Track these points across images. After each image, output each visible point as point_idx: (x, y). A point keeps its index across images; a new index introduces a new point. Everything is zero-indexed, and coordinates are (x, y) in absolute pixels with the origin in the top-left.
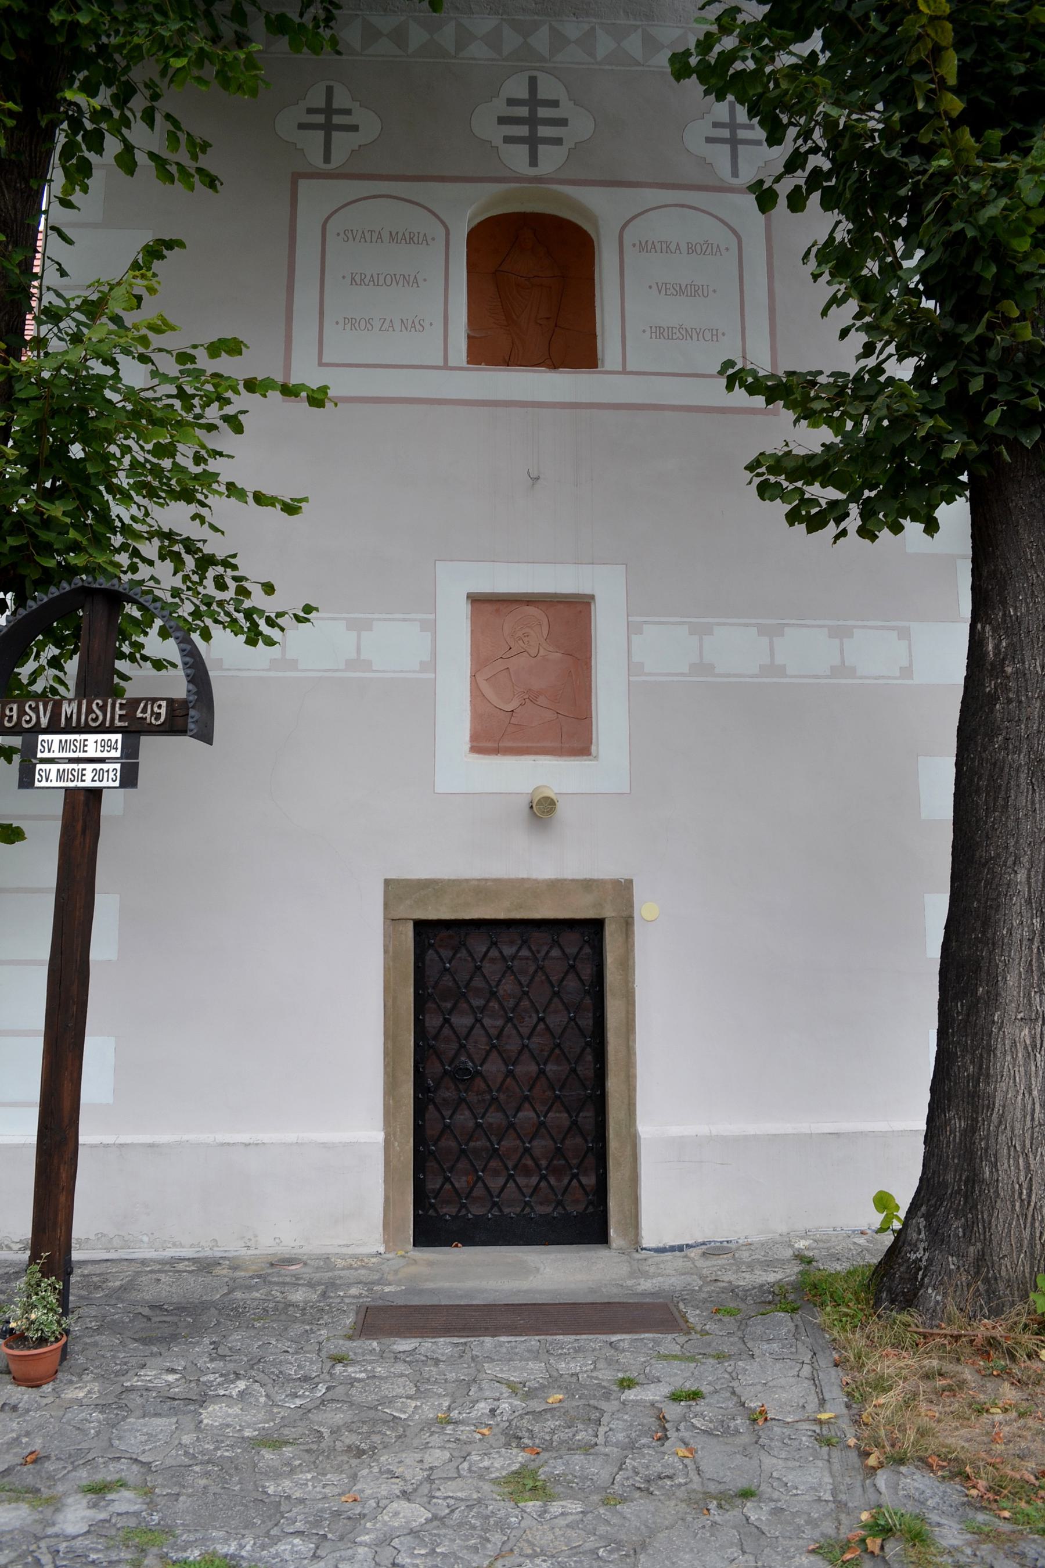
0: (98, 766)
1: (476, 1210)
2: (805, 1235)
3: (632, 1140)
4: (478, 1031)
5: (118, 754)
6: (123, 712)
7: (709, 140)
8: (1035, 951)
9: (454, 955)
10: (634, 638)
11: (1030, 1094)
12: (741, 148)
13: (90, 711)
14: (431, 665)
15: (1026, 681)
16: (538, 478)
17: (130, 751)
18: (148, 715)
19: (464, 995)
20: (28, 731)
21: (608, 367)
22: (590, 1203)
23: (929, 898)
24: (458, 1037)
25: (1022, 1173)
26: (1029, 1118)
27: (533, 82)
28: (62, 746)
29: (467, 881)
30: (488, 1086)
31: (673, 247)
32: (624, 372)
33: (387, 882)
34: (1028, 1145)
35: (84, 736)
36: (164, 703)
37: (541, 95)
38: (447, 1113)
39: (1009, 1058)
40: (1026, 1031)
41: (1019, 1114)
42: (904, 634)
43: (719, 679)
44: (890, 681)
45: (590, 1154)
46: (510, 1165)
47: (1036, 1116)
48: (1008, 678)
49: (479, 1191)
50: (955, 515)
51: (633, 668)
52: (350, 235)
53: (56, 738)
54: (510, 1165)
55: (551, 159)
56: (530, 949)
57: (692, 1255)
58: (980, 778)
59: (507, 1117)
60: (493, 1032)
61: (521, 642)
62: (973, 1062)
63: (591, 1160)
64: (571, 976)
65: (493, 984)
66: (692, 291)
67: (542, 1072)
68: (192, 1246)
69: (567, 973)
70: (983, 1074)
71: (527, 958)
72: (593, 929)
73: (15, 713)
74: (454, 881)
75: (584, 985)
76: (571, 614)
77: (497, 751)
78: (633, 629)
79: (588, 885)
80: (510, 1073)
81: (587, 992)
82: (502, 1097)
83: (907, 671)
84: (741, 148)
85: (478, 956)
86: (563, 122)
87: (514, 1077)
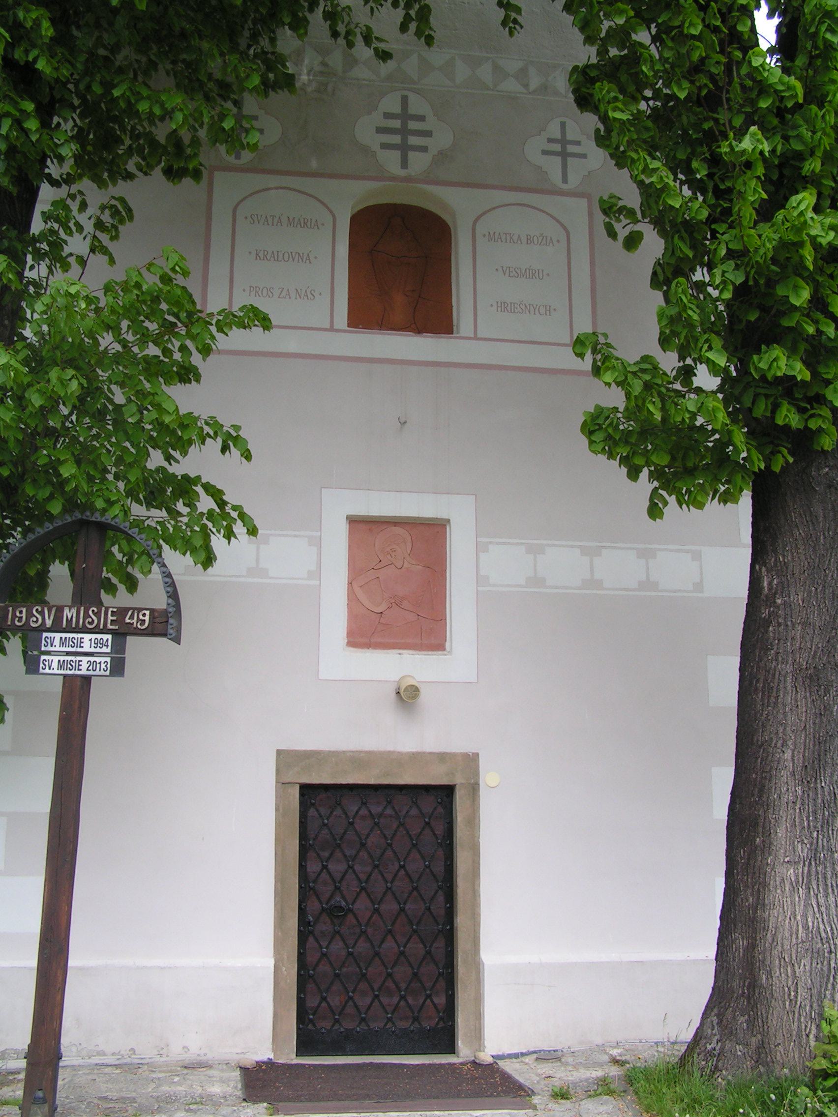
0: (92, 659)
1: (348, 1024)
2: (617, 1045)
3: (477, 966)
4: (350, 876)
5: (109, 650)
6: (114, 618)
7: (545, 152)
8: (798, 811)
9: (331, 813)
10: (483, 556)
11: (795, 918)
12: (570, 160)
13: (86, 615)
14: (316, 574)
15: (791, 610)
16: (405, 422)
17: (119, 648)
18: (135, 621)
19: (339, 846)
20: (35, 629)
21: (463, 333)
22: (441, 1019)
23: (715, 770)
24: (333, 880)
25: (790, 979)
26: (794, 936)
27: (405, 100)
28: (63, 642)
29: (344, 752)
30: (358, 921)
31: (515, 238)
32: (476, 338)
33: (279, 753)
34: (794, 958)
35: (80, 635)
36: (148, 613)
37: (412, 111)
38: (324, 944)
39: (779, 891)
40: (792, 871)
41: (787, 934)
42: (697, 556)
43: (548, 591)
44: (685, 594)
45: (441, 978)
46: (376, 987)
47: (800, 936)
48: (778, 607)
49: (350, 1010)
50: (746, 501)
51: (481, 580)
52: (255, 219)
53: (57, 636)
54: (376, 987)
55: (419, 162)
56: (393, 808)
57: (527, 1061)
58: (758, 681)
59: (374, 947)
60: (363, 877)
61: (389, 556)
62: (752, 895)
63: (442, 984)
64: (427, 831)
65: (364, 837)
66: (531, 274)
67: (402, 910)
68: (113, 1054)
69: (423, 829)
70: (760, 904)
71: (391, 816)
72: (445, 794)
73: (24, 615)
74: (334, 752)
75: (437, 838)
76: (430, 534)
77: (368, 645)
78: (480, 548)
79: (443, 757)
80: (376, 910)
81: (440, 845)
82: (370, 930)
83: (699, 586)
84: (570, 160)
85: (351, 814)
86: (428, 134)
87: (380, 914)
